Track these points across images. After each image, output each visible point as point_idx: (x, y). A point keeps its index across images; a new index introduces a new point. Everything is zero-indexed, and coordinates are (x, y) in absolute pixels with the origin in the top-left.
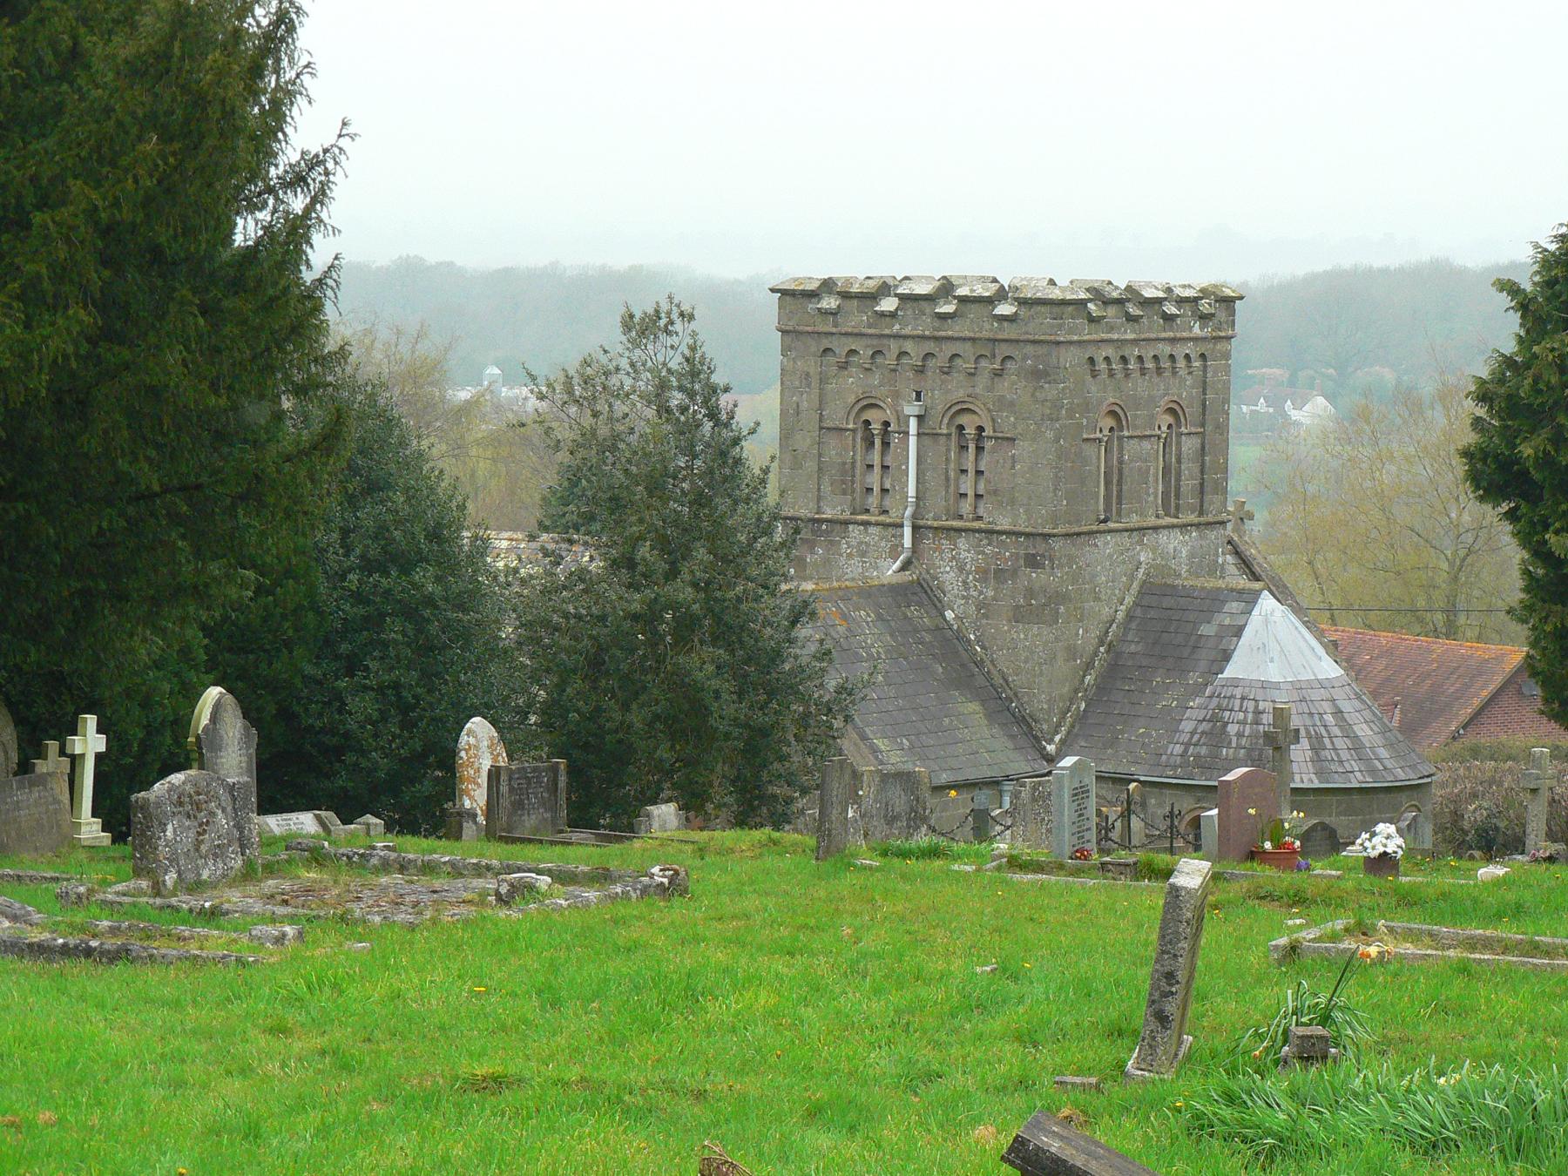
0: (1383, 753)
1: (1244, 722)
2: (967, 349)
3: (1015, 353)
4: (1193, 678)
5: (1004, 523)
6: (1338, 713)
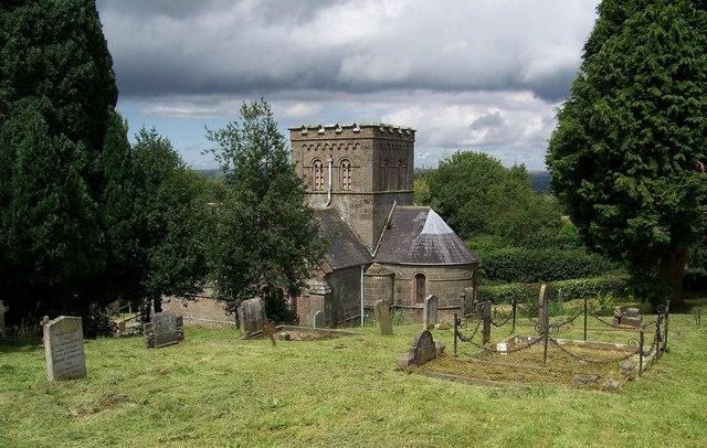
2: (346, 142)
3: (359, 141)
5: (358, 191)
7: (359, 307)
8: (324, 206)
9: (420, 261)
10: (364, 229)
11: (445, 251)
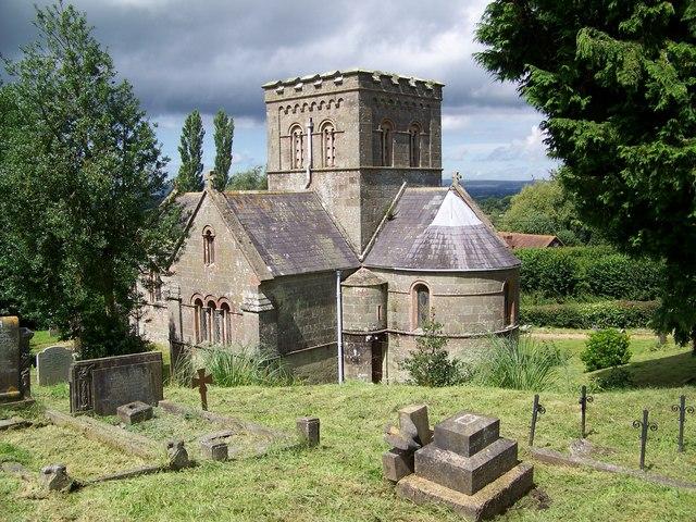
0: (498, 255)
1: (437, 244)
4: (419, 226)
5: (342, 166)
6: (479, 238)
7: (334, 332)
8: (303, 188)
9: (421, 264)
10: (349, 219)
11: (460, 253)
